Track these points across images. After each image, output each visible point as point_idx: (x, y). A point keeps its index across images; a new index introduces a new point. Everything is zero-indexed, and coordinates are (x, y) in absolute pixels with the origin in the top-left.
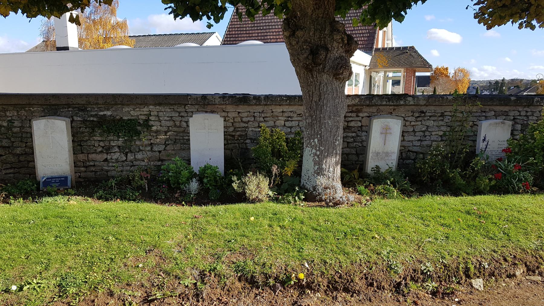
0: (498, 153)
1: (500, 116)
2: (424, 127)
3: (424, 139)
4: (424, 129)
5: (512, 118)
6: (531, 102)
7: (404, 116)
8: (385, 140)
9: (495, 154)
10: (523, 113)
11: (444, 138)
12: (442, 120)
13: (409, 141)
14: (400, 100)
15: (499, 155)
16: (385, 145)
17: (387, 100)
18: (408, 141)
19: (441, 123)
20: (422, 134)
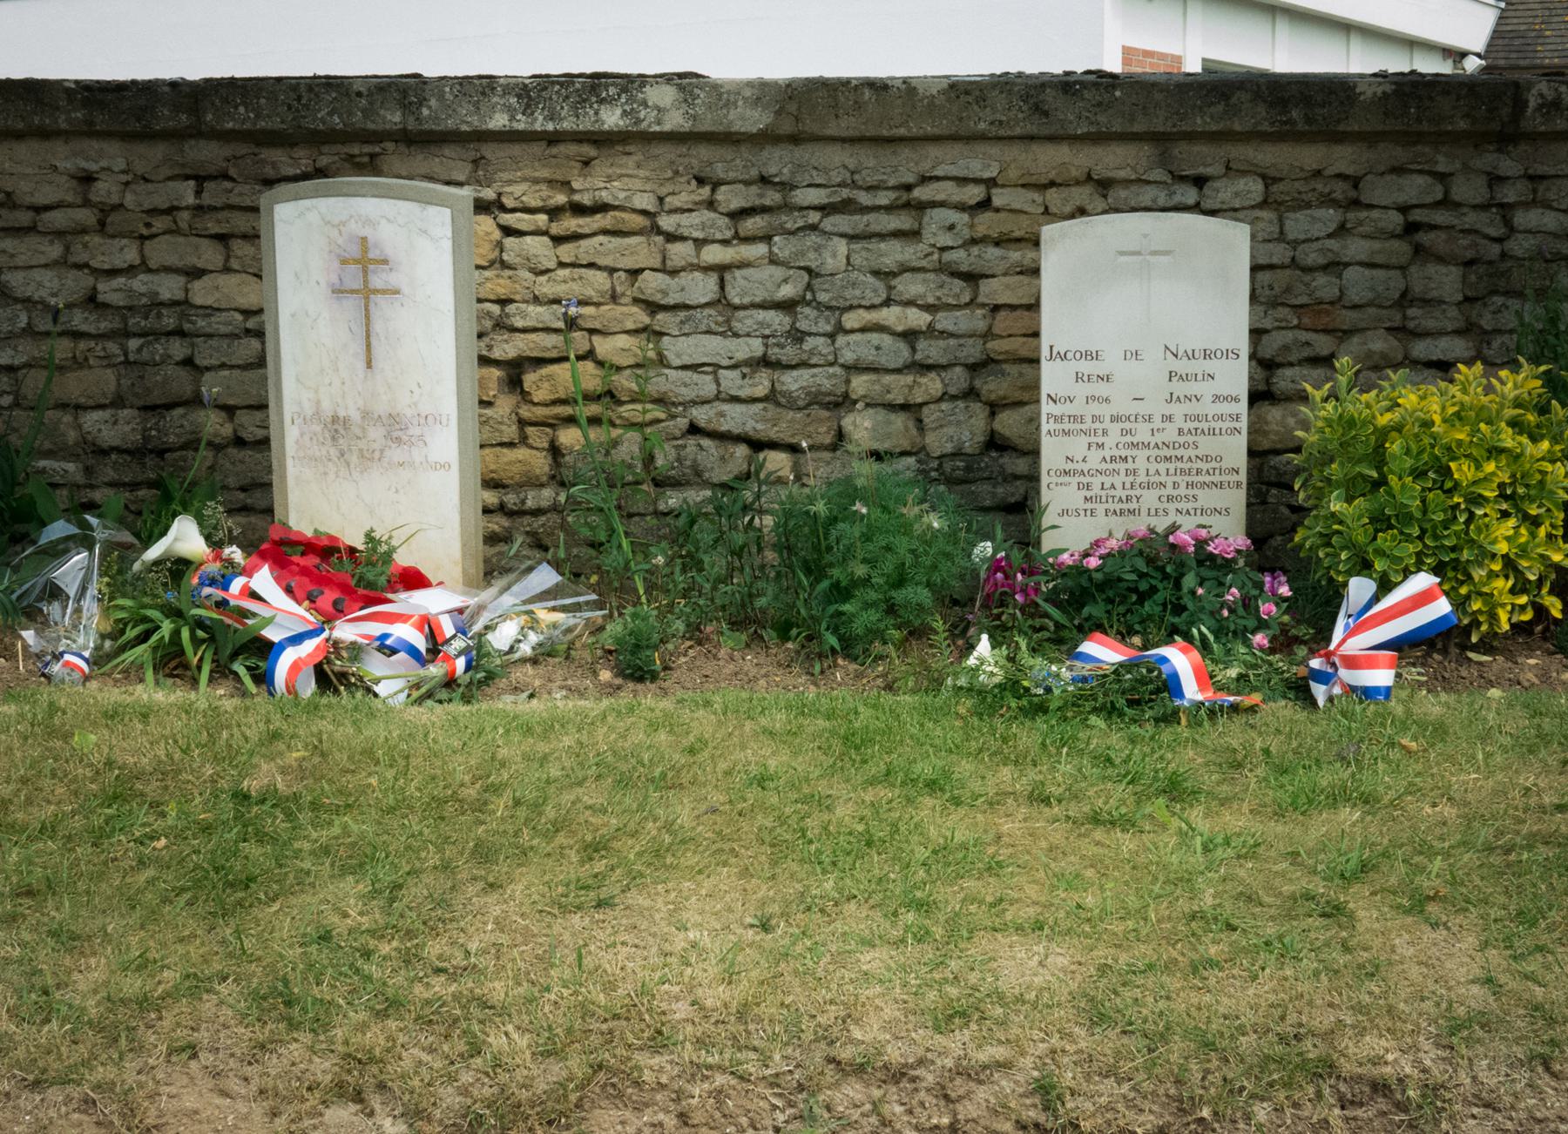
0: (1170, 434)
1: (1308, 206)
2: (785, 281)
3: (789, 353)
4: (787, 291)
5: (1395, 220)
6: (1505, 112)
7: (651, 208)
8: (368, 336)
9: (1146, 438)
10: (1468, 190)
11: (930, 350)
12: (913, 235)
13: (693, 367)
14: (602, 101)
15: (1184, 446)
16: (369, 365)
17: (513, 100)
18: (684, 367)
19: (893, 253)
20: (777, 320)
